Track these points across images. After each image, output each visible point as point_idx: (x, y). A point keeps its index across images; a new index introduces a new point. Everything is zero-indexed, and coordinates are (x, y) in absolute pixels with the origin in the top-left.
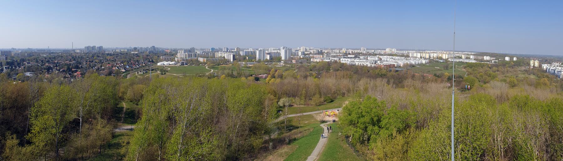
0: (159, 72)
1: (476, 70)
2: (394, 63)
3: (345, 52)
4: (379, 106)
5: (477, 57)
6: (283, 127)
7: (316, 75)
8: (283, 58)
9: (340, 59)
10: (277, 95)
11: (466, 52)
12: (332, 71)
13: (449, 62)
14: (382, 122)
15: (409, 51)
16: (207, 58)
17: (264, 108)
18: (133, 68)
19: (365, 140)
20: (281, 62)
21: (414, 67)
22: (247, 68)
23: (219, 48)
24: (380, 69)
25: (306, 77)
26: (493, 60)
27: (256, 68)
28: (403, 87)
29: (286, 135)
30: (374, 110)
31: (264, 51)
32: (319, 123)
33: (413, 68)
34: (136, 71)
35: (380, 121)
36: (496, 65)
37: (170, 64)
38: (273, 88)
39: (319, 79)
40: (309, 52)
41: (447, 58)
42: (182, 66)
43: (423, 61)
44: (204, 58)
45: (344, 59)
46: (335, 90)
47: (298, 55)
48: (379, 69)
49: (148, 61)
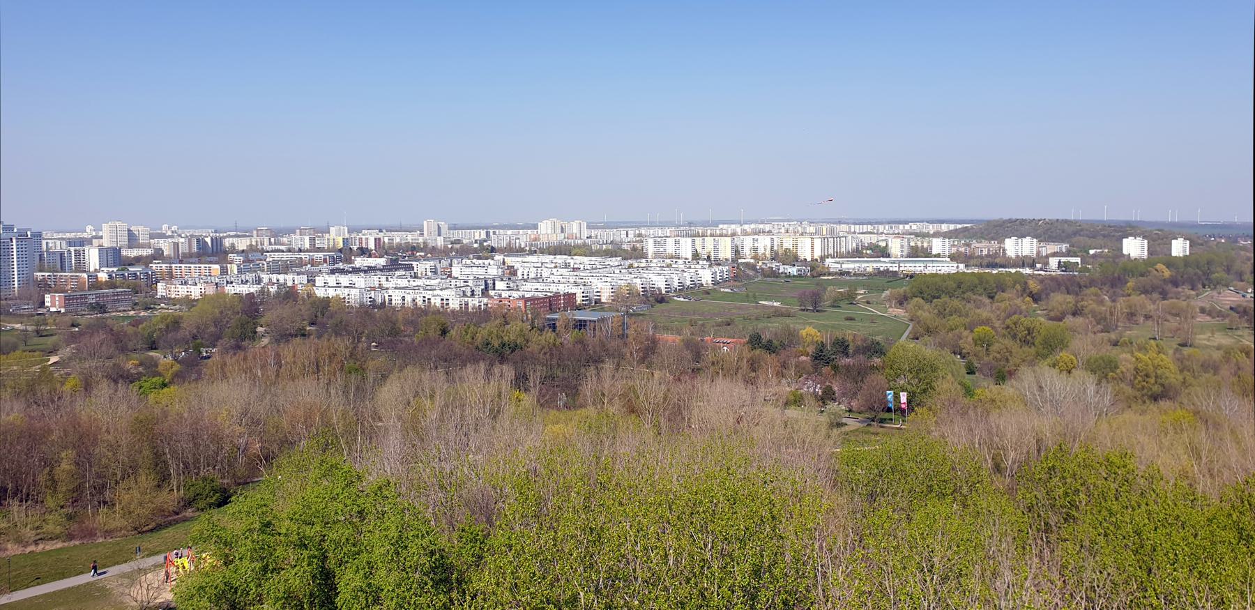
1: (956, 311)
2: (573, 290)
3: (341, 245)
5: (968, 245)
7: (177, 367)
9: (311, 281)
11: (915, 222)
12: (265, 341)
13: (830, 274)
15: (643, 232)
21: (663, 306)
26: (1054, 255)
36: (1069, 283)
40: (150, 251)
41: (817, 254)
43: (700, 272)
45: (332, 280)
47: (81, 267)
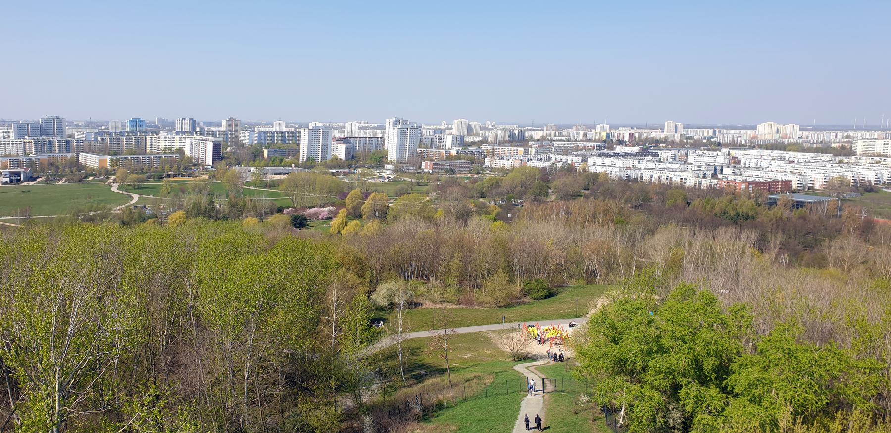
2: (789, 177)
3: (604, 138)
4: (724, 324)
6: (396, 371)
7: (499, 210)
8: (392, 156)
9: (584, 161)
10: (368, 272)
12: (553, 198)
14: (733, 376)
15: (852, 134)
16: (115, 155)
17: (326, 312)
19: (674, 427)
20: (383, 167)
21: (872, 195)
22: (266, 186)
24: (729, 197)
25: (464, 216)
27: (297, 186)
28: (821, 263)
29: (408, 391)
30: (705, 335)
31: (327, 130)
32: (510, 360)
33: (867, 195)
35: (727, 374)
38: (355, 249)
39: (509, 224)
40: (480, 138)
42: (14, 185)
44: (105, 154)
45: (599, 161)
46: (563, 260)
48: (727, 194)
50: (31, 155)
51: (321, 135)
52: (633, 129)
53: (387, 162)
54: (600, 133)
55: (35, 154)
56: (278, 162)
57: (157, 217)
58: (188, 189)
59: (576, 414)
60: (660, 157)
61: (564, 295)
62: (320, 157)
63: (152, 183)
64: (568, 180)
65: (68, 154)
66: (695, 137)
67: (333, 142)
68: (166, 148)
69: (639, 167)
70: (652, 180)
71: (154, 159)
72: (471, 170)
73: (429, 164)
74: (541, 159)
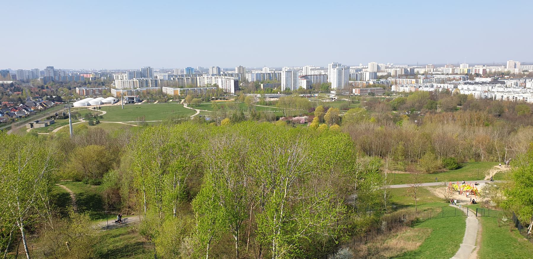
0: (82, 121)
8: (334, 86)
9: (456, 87)
16: (182, 88)
18: (14, 117)
20: (330, 92)
22: (267, 105)
23: (200, 68)
32: (443, 202)
34: (25, 122)
37: (102, 103)
40: (386, 74)
42: (131, 105)
44: (176, 87)
45: (465, 87)
49: (47, 99)
50: (137, 88)
51: (292, 74)
52: (485, 66)
53: (331, 89)
54: (463, 70)
55: (140, 88)
56: (270, 91)
57: (215, 122)
58: (226, 106)
59: (500, 227)
60: (506, 84)
61: (467, 167)
62: (292, 87)
63: (205, 103)
64: (449, 99)
65: (156, 88)
66: (530, 71)
67: (299, 79)
68: (208, 84)
69: (493, 91)
70: (503, 99)
71: (197, 90)
72: (384, 93)
73: (357, 90)
74: (427, 86)
